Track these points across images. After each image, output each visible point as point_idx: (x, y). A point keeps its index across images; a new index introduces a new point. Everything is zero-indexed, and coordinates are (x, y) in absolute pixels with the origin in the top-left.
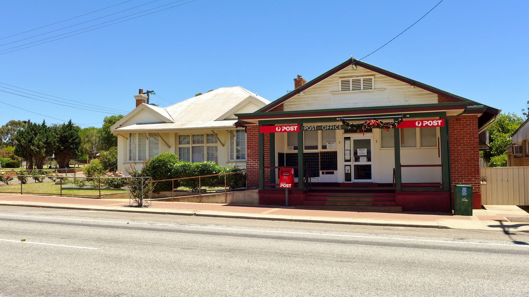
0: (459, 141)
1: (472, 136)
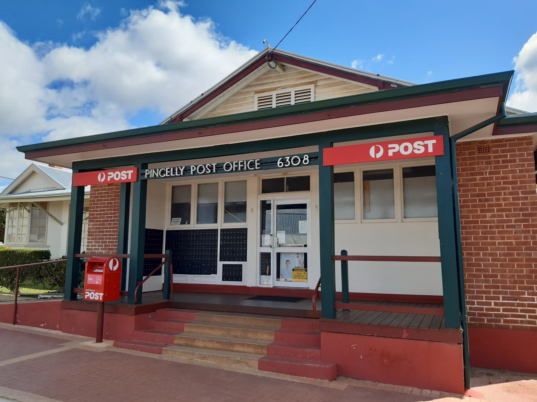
0: (487, 200)
1: (520, 188)
